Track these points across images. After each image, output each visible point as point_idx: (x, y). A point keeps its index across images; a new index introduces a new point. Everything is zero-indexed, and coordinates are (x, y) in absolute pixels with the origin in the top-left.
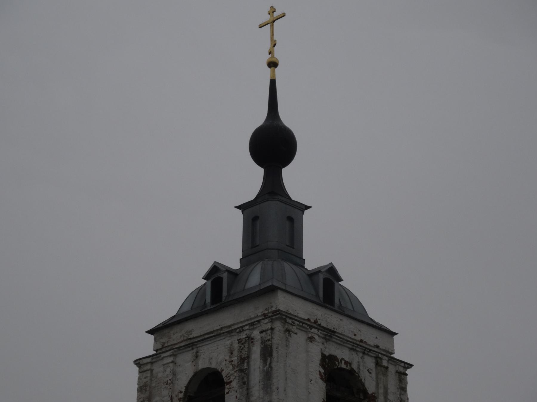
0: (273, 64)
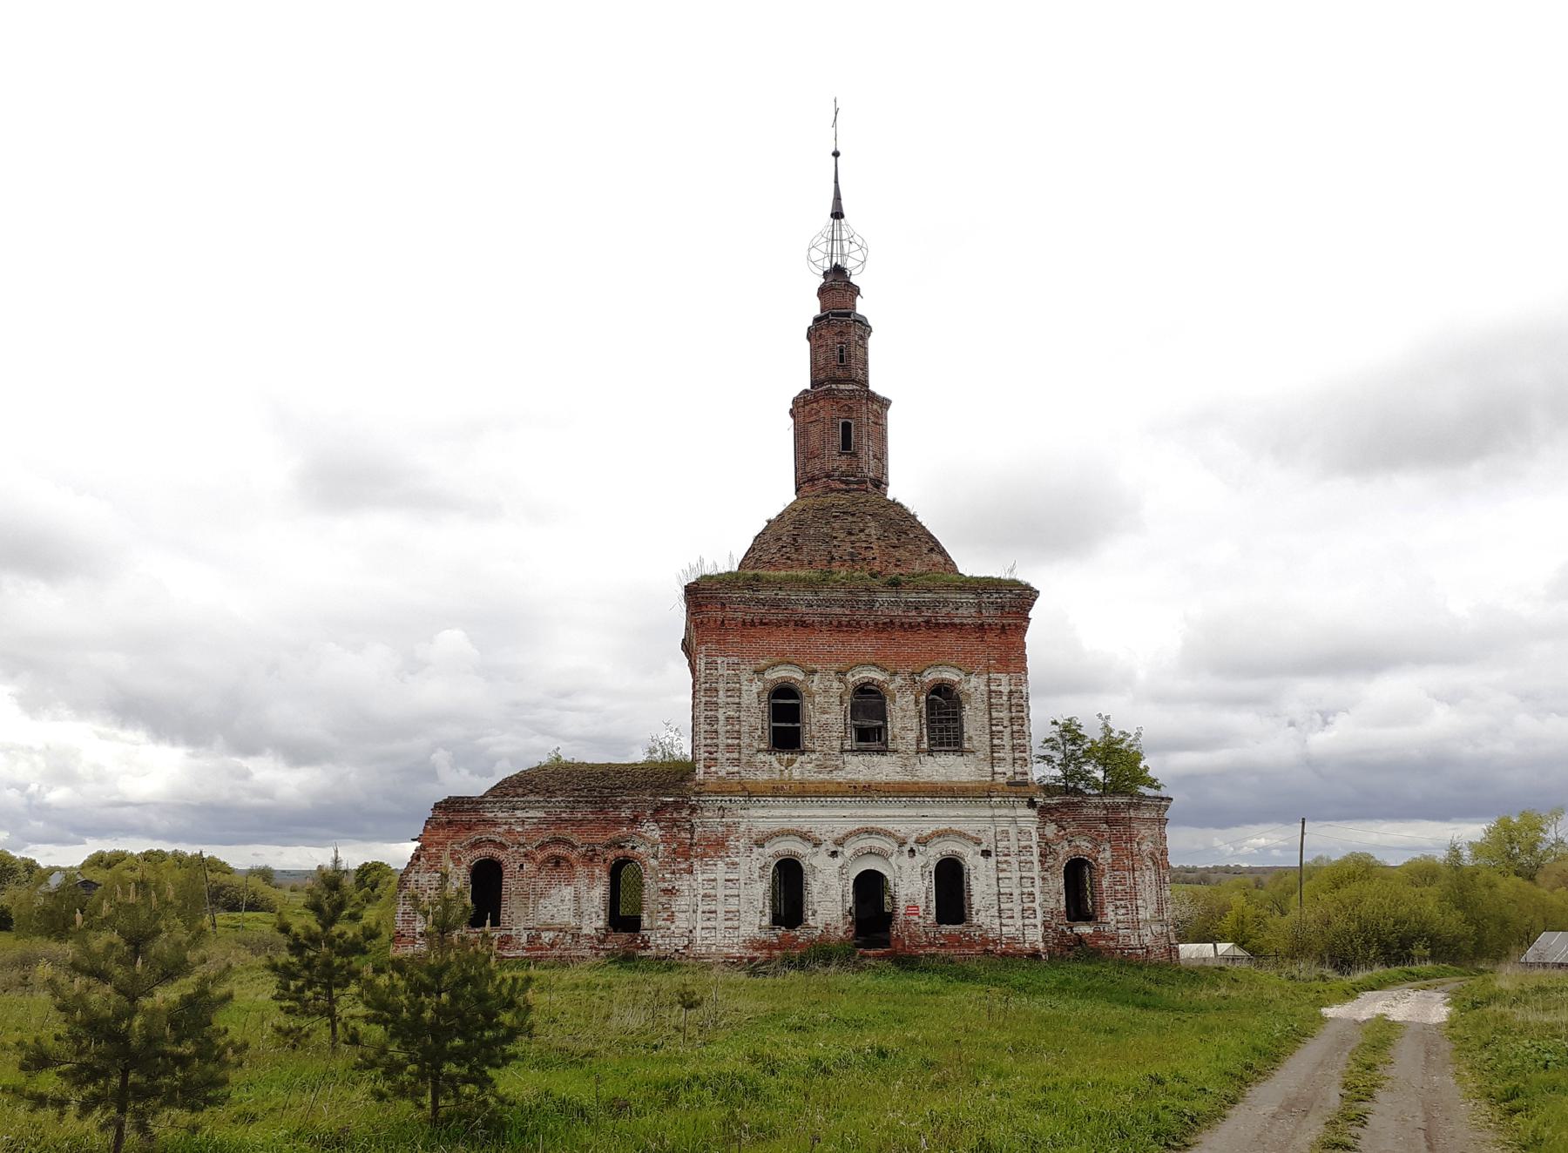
0: (836, 154)
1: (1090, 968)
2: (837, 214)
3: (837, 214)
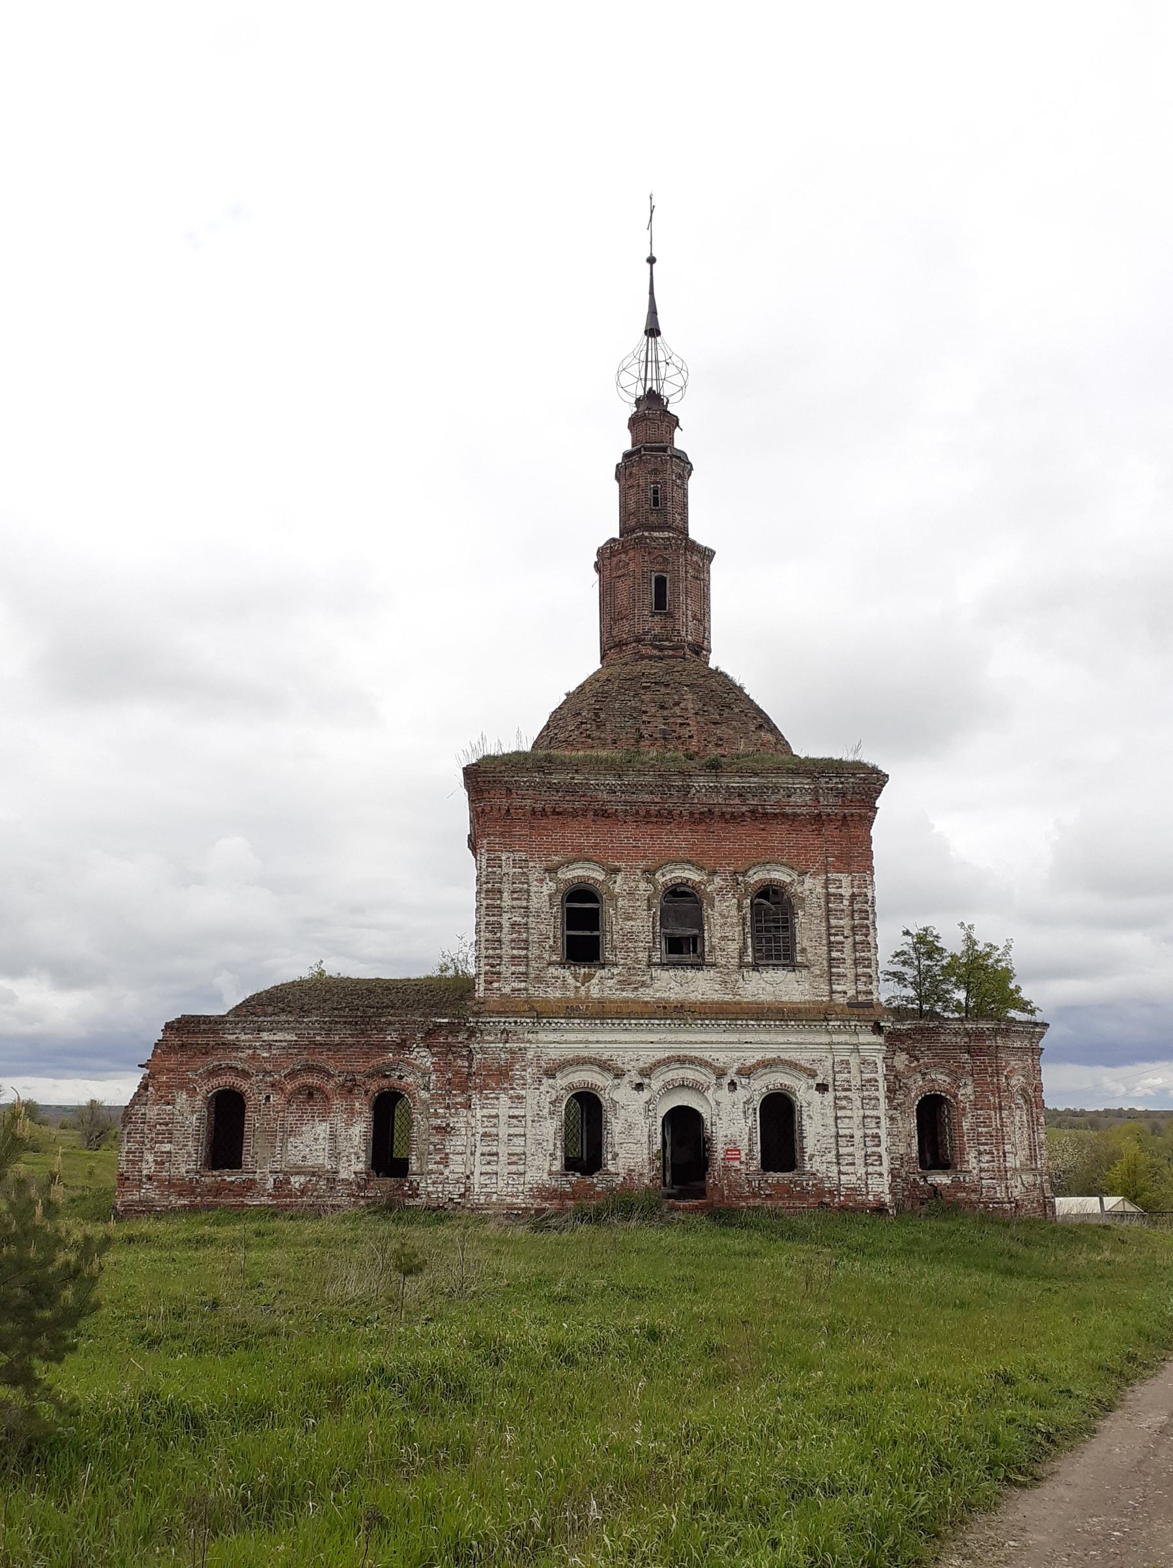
0: (651, 260)
1: (945, 1226)
2: (653, 331)
3: (653, 331)
